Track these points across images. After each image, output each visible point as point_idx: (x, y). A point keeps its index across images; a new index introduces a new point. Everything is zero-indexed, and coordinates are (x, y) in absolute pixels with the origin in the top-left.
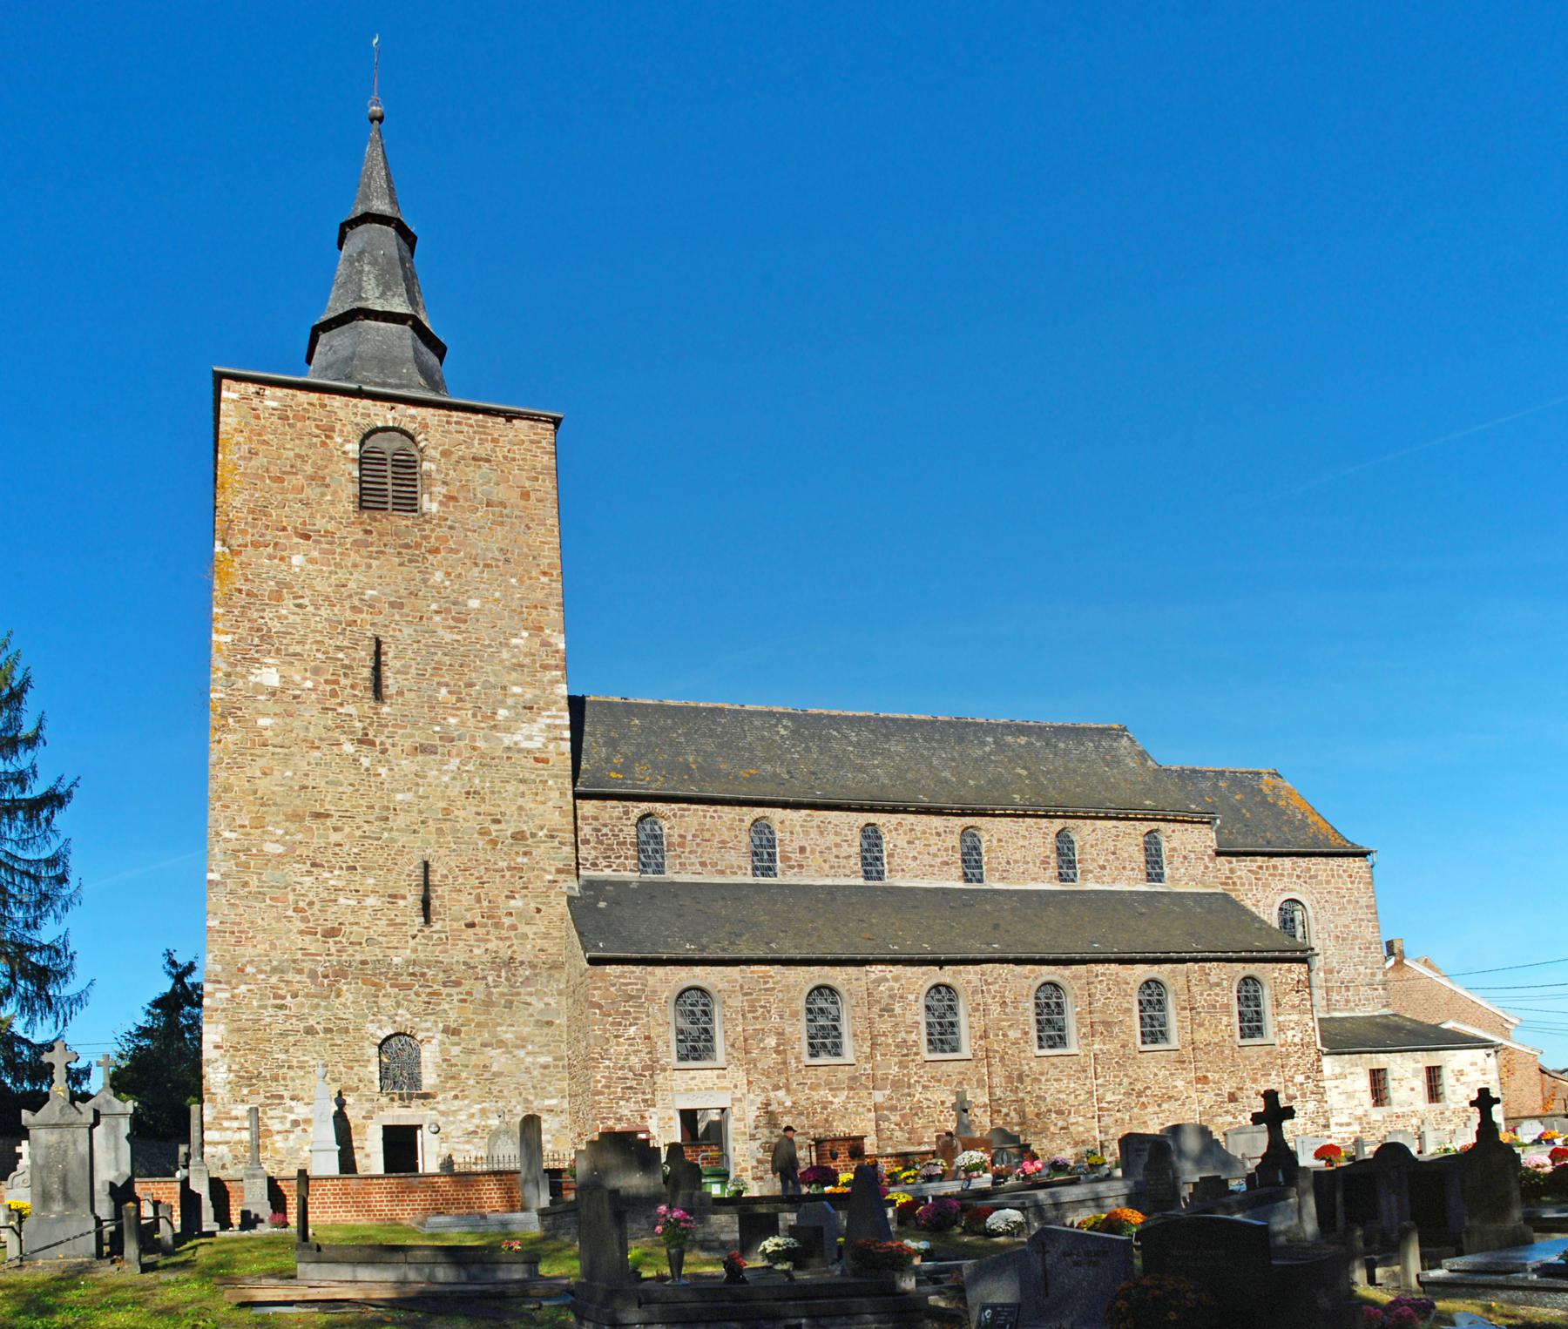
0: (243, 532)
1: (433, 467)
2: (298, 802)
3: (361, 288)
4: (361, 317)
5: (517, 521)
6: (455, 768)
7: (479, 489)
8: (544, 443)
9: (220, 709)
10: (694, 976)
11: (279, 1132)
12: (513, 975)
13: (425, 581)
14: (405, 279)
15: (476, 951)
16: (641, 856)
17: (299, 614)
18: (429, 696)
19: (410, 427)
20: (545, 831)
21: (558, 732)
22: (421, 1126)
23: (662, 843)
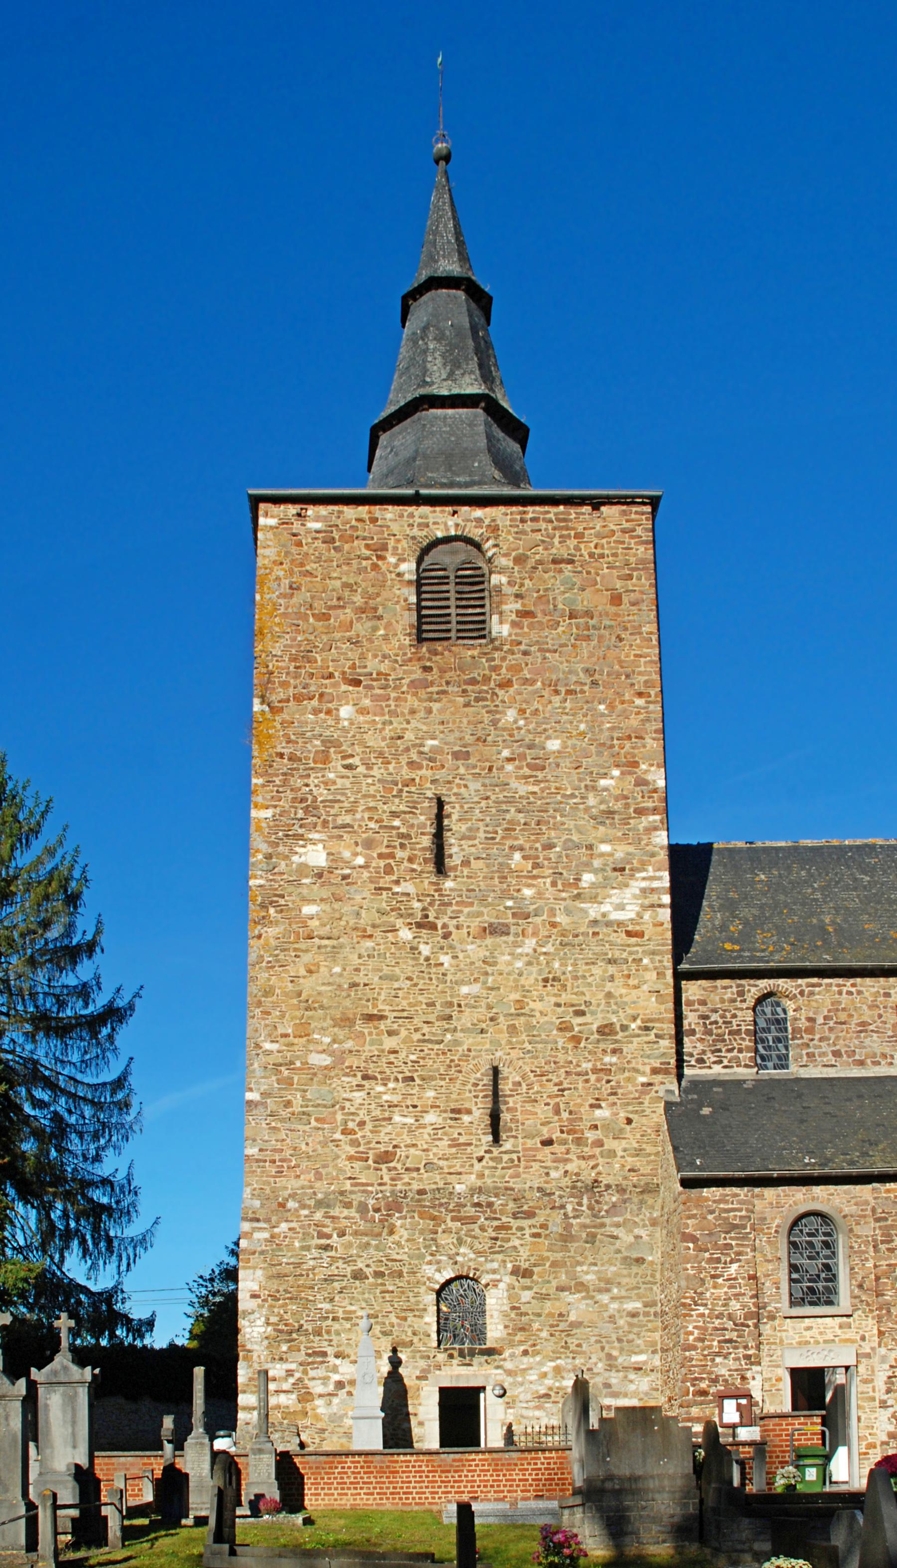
0: (285, 685)
1: (504, 580)
2: (347, 1003)
3: (425, 371)
4: (426, 406)
5: (606, 633)
6: (530, 951)
7: (560, 599)
8: (639, 531)
9: (259, 899)
10: (813, 1199)
11: (320, 1396)
12: (597, 1202)
13: (495, 723)
14: (477, 351)
15: (554, 1174)
16: (760, 1047)
17: (348, 777)
18: (500, 864)
19: (475, 533)
20: (639, 1022)
21: (656, 896)
22: (484, 1388)
23: (786, 1030)
